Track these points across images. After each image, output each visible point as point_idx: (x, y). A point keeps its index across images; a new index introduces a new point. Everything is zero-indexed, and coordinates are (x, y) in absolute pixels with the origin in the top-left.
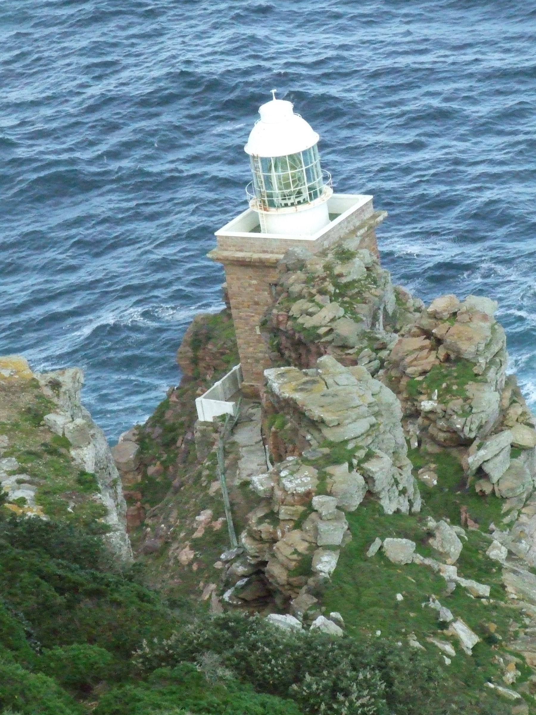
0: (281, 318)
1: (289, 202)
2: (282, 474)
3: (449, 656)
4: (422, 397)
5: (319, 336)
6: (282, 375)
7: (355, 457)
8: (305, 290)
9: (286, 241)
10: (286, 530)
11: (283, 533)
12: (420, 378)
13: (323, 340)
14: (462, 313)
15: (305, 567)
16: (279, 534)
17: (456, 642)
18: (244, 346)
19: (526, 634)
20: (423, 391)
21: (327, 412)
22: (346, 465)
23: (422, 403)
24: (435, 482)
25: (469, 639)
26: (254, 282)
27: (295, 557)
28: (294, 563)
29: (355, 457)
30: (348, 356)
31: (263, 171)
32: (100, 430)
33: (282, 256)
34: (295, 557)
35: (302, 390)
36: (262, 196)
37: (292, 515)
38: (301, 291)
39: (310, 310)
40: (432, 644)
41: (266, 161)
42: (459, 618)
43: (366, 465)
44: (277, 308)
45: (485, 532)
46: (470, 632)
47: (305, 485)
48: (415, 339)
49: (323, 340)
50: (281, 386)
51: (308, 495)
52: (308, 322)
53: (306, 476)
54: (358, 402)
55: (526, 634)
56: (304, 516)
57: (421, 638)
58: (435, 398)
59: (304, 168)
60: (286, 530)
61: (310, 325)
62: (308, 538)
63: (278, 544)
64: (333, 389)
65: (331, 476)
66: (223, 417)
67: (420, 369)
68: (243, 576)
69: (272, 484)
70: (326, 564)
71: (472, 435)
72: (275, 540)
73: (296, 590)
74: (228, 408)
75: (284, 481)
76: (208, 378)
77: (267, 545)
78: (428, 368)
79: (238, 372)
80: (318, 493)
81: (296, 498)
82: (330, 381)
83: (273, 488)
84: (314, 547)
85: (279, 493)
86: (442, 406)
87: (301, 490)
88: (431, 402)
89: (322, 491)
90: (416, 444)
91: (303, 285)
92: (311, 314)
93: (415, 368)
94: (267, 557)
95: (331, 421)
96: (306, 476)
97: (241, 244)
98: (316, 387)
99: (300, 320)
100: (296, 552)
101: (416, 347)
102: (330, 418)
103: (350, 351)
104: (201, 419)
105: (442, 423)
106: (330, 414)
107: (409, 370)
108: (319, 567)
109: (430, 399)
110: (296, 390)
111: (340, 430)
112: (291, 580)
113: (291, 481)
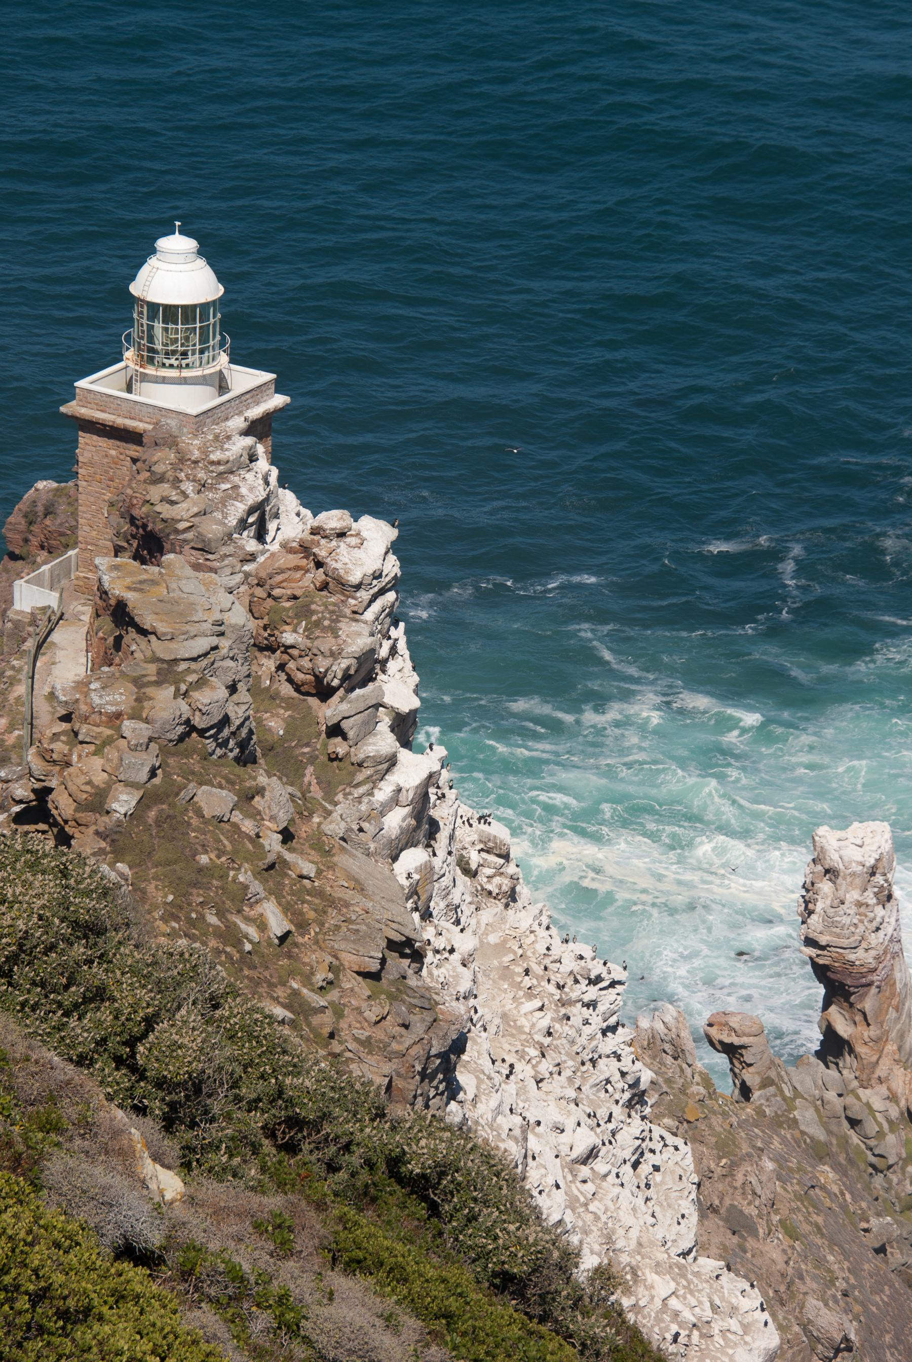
0: (135, 502)
1: (167, 362)
2: (92, 686)
3: (250, 941)
4: (287, 628)
5: (177, 532)
6: (116, 568)
7: (184, 681)
8: (170, 473)
9: (161, 409)
10: (84, 754)
11: (80, 756)
12: (288, 605)
13: (181, 537)
14: (352, 535)
15: (97, 802)
16: (75, 758)
17: (262, 926)
18: (87, 528)
19: (349, 930)
20: (288, 621)
21: (162, 621)
22: (172, 689)
23: (284, 635)
24: (281, 732)
25: (277, 924)
26: (113, 452)
27: (88, 788)
28: (85, 796)
29: (184, 681)
30: (208, 563)
31: (148, 319)
32: (442, 872)
33: (151, 427)
34: (88, 788)
35: (135, 590)
36: (139, 349)
37: (95, 738)
38: (165, 473)
39: (174, 498)
40: (235, 924)
41: (154, 307)
42: (273, 898)
43: (195, 695)
44: (132, 488)
45: (330, 803)
46: (281, 916)
47: (117, 704)
48: (291, 556)
49: (181, 537)
50: (113, 581)
51: (118, 715)
52: (166, 511)
53: (121, 694)
54: (200, 615)
55: (349, 930)
56: (108, 742)
57: (220, 914)
58: (301, 631)
59: (198, 325)
60: (84, 754)
61: (168, 516)
62: (108, 769)
63: (71, 769)
64: (175, 595)
65: (150, 699)
66: (44, 609)
67: (289, 592)
68: (20, 802)
69: (78, 696)
70: (123, 803)
71: (336, 683)
72: (68, 764)
73: (82, 828)
74: (51, 599)
75: (93, 694)
76: (39, 559)
77: (58, 768)
78: (298, 593)
79: (73, 559)
80: (132, 718)
81: (104, 718)
82: (173, 586)
83: (77, 701)
84: (115, 779)
85: (83, 708)
86: (308, 643)
87: (111, 709)
88: (295, 635)
89: (135, 715)
90: (268, 682)
91: (169, 467)
92: (173, 503)
93: (284, 591)
94: (53, 783)
95: (165, 634)
96: (121, 694)
97: (105, 401)
98: (154, 589)
99: (158, 508)
100: (89, 783)
101: (292, 565)
102: (164, 630)
103: (210, 556)
104: (17, 606)
105: (305, 663)
106: (164, 624)
107: (276, 592)
108: (115, 806)
109: (295, 631)
110: (129, 588)
111: (173, 645)
112: (78, 815)
113: (101, 696)
